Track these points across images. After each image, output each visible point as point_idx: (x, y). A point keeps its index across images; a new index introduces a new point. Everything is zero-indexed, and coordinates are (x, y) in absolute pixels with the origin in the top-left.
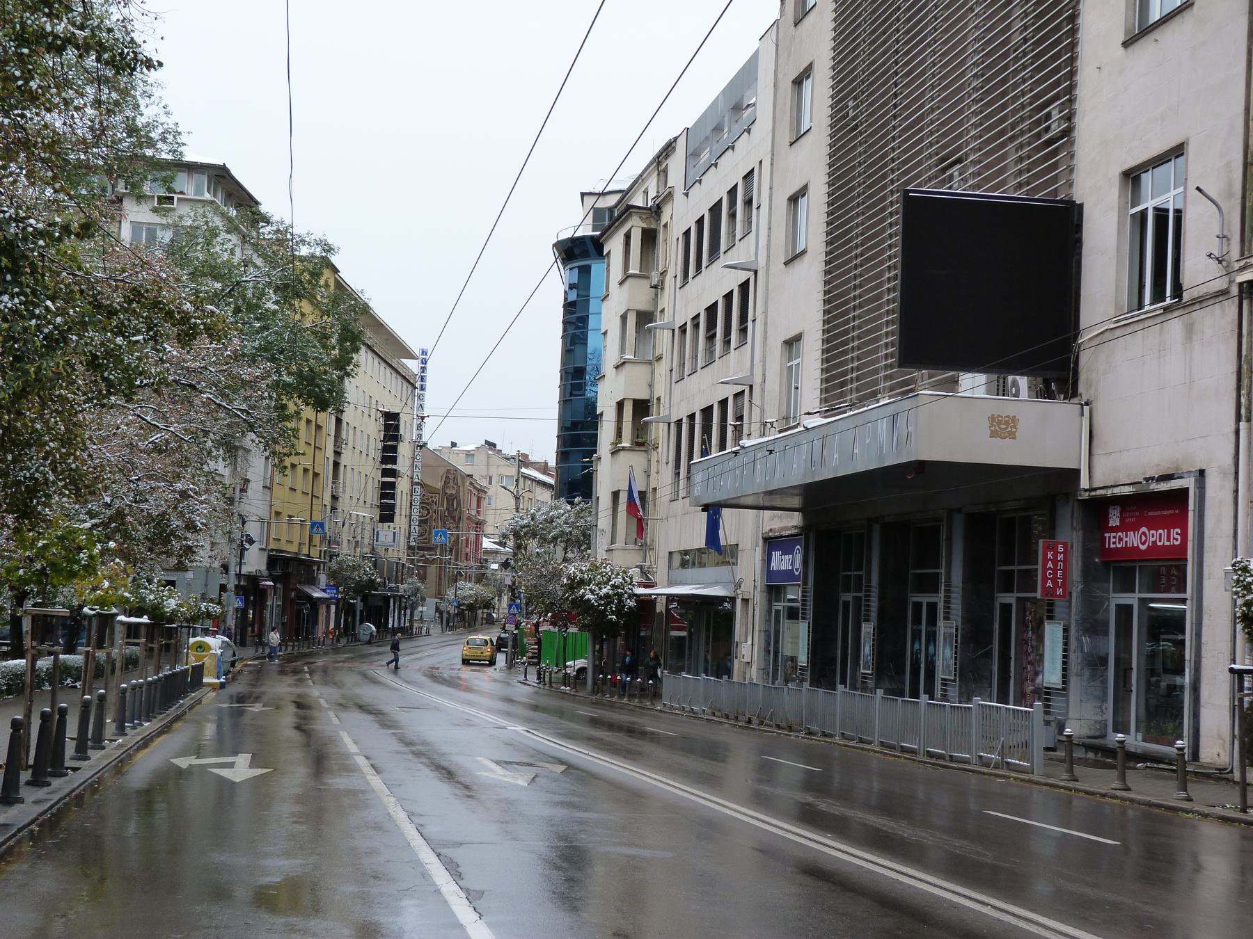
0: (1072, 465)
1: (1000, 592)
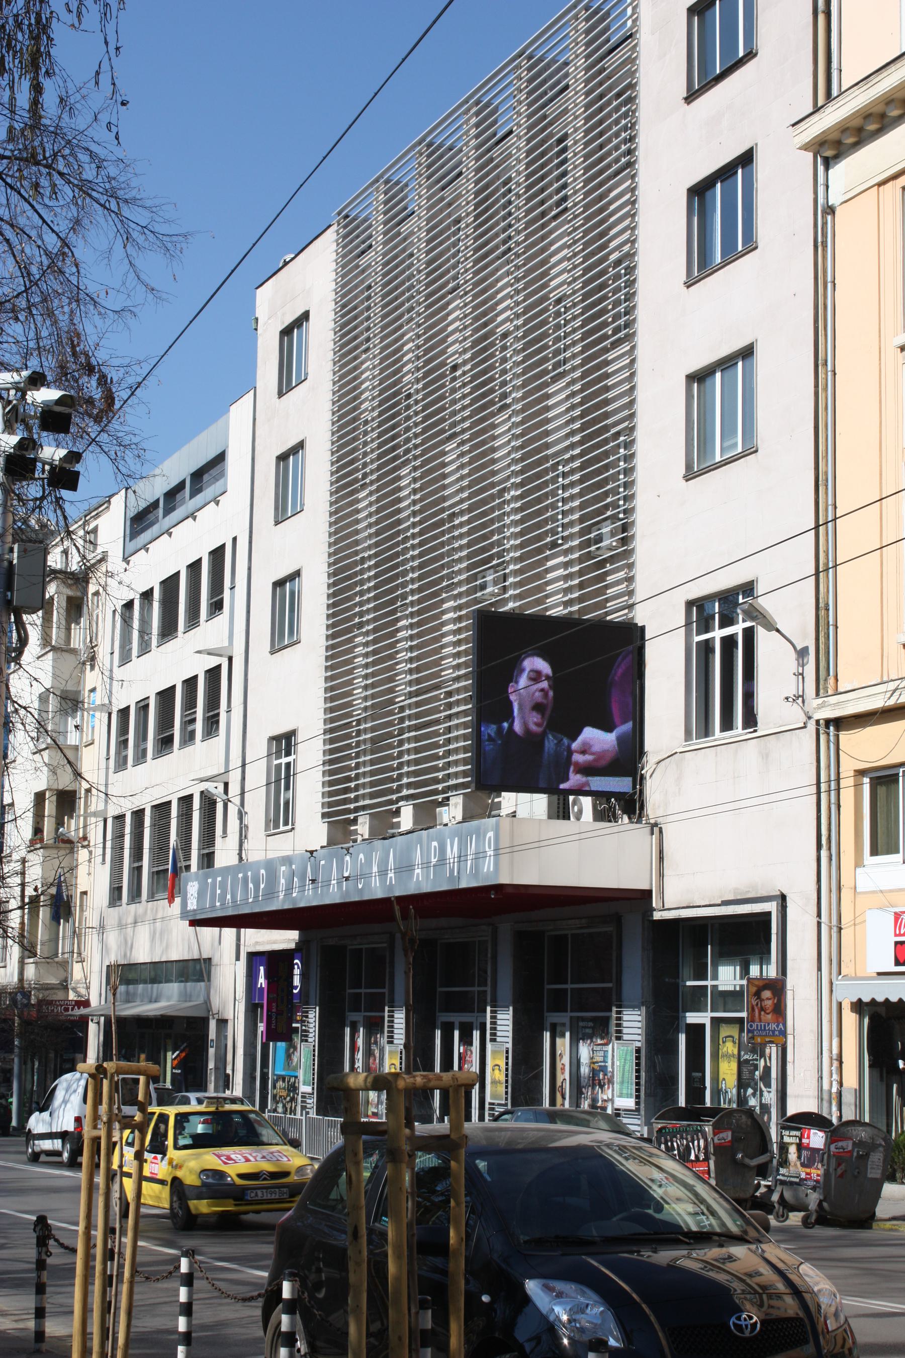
0: (645, 886)
1: (350, 1011)
